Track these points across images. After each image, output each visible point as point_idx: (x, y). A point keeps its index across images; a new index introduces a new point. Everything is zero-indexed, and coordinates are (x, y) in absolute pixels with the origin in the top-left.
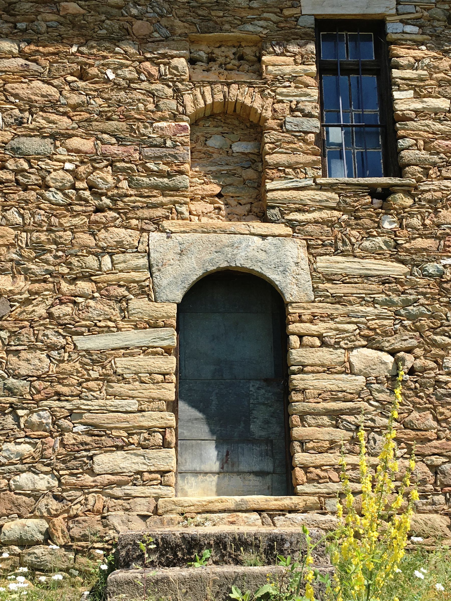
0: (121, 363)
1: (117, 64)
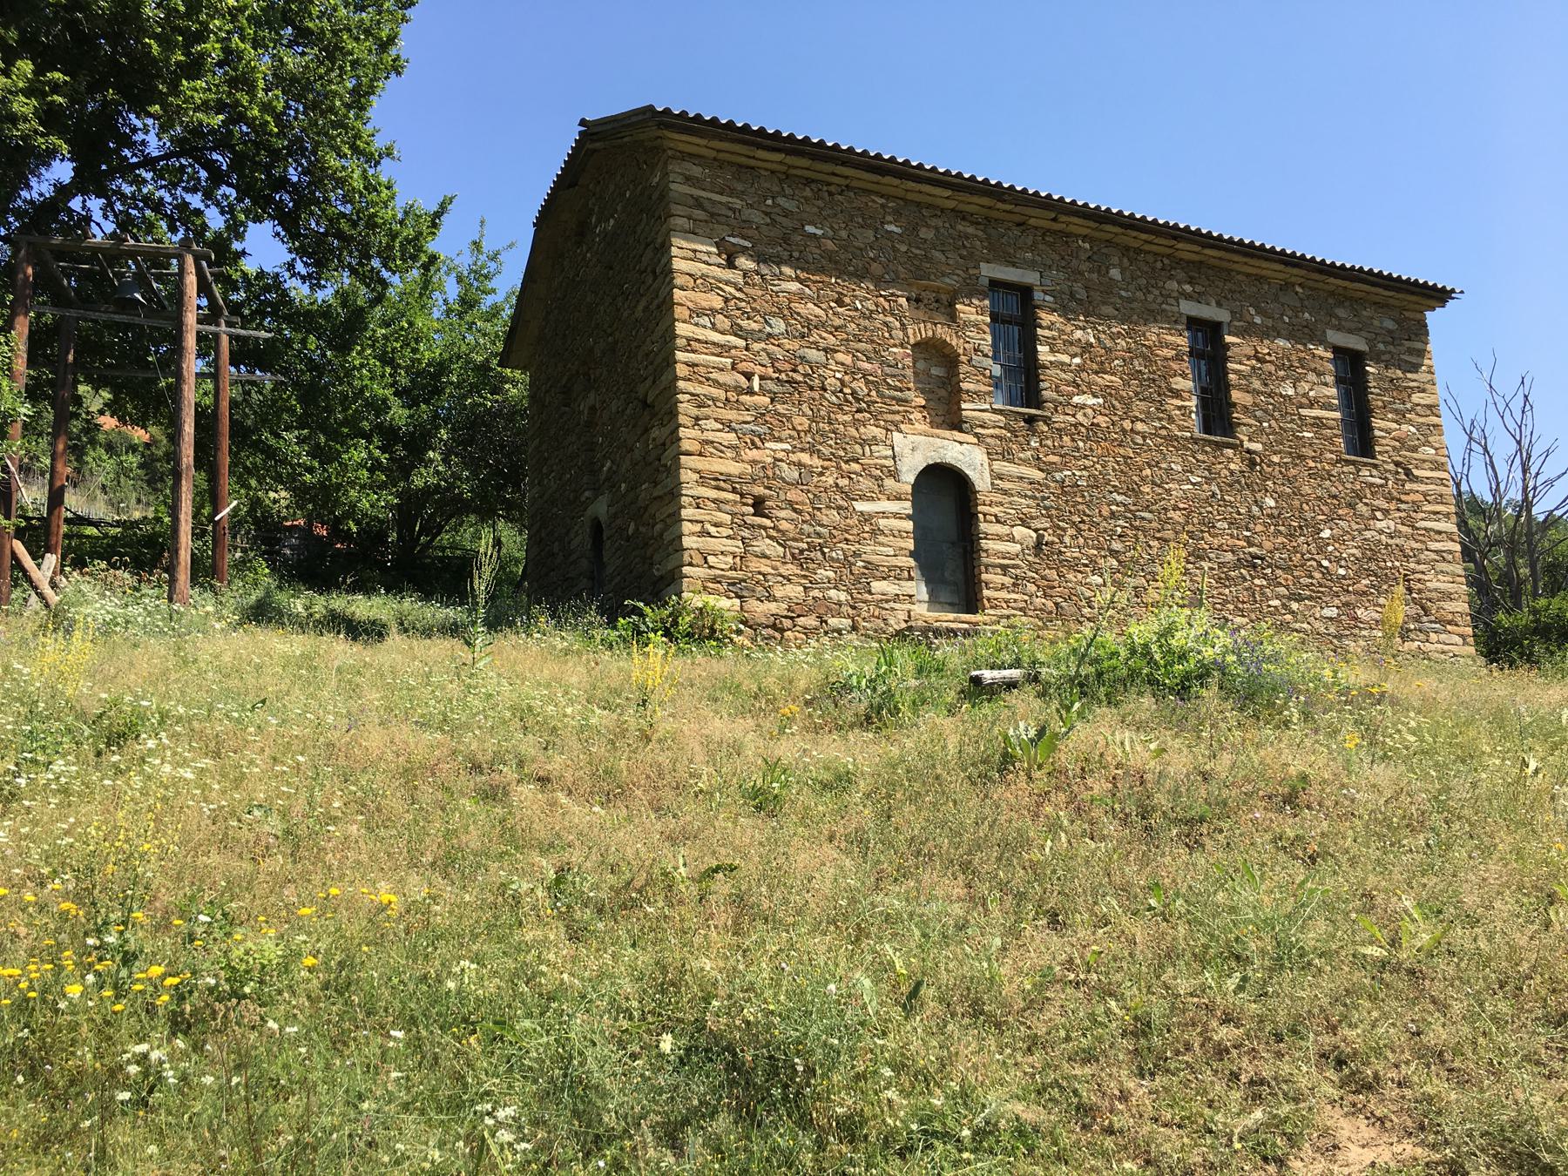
0: (882, 522)
1: (863, 296)
